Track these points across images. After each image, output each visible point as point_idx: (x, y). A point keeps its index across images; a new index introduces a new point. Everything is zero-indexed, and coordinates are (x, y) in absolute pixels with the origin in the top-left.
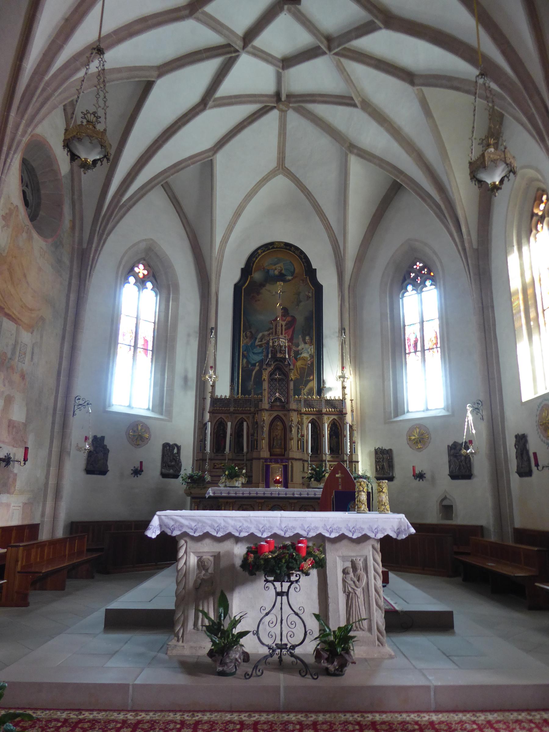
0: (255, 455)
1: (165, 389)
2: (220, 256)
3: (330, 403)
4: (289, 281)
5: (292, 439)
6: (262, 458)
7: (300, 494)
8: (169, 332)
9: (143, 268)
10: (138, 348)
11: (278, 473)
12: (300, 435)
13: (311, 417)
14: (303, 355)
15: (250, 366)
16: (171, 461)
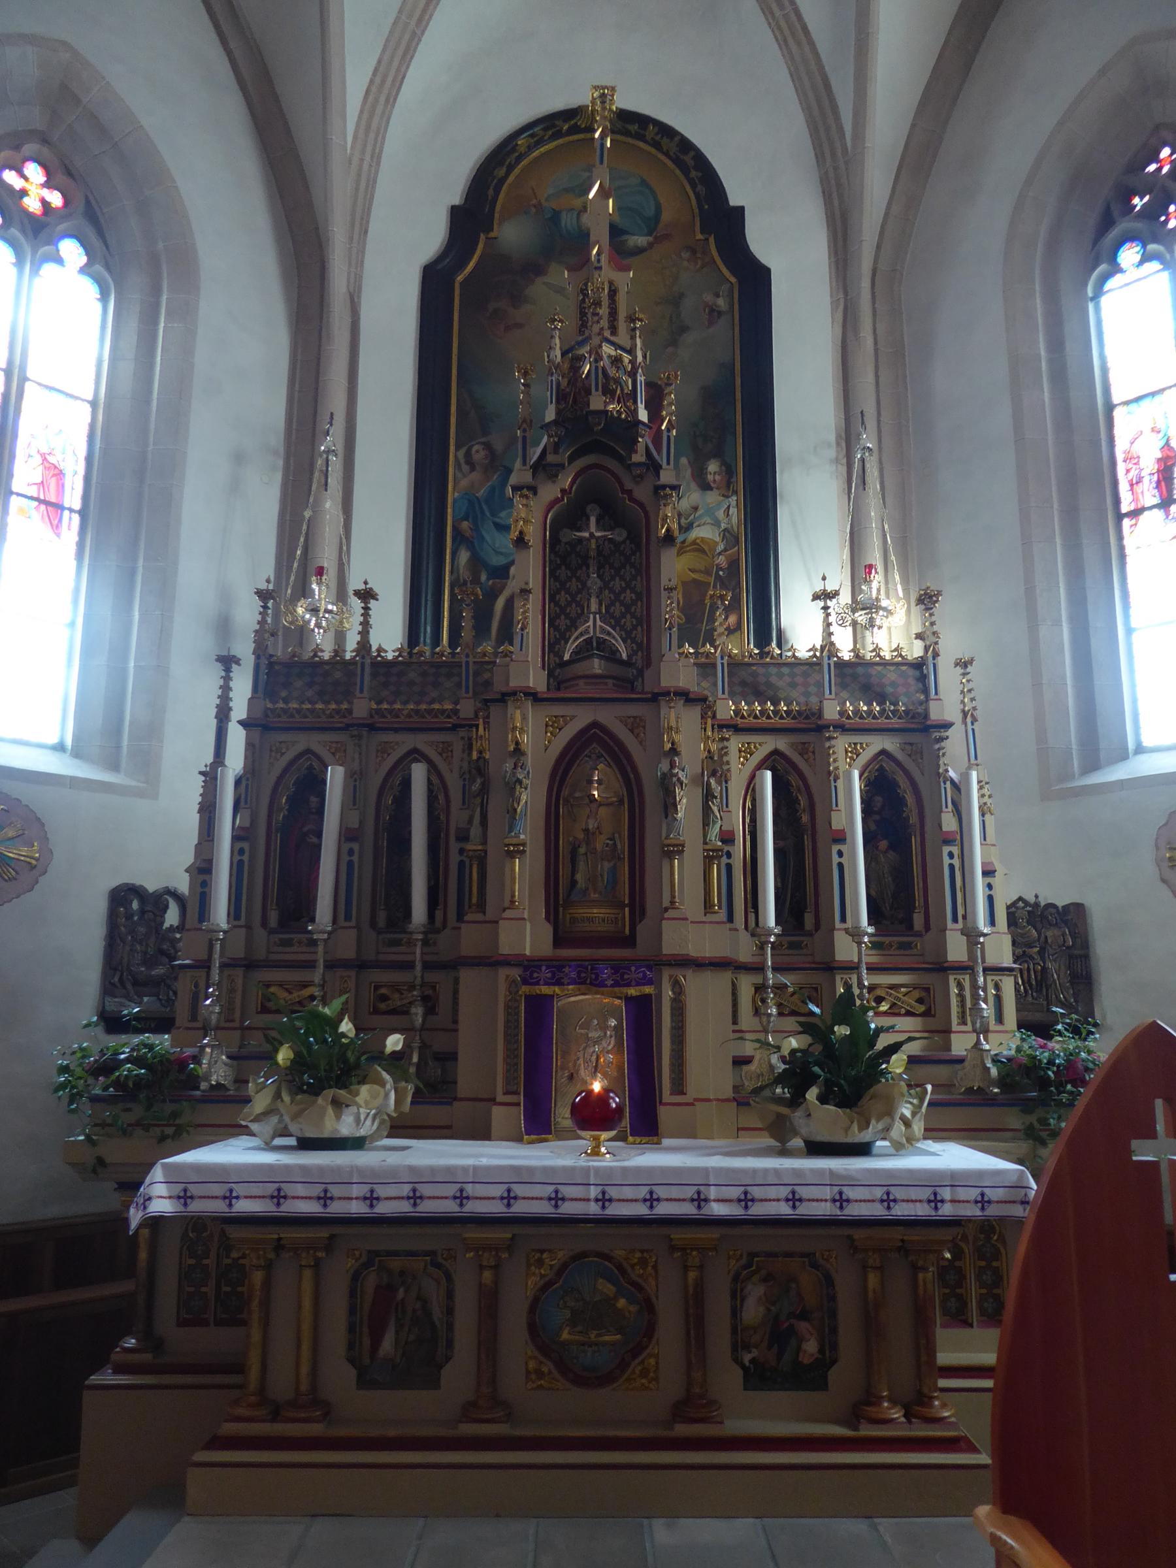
0: (470, 940)
1: (132, 664)
2: (363, 152)
3: (855, 677)
4: (639, 251)
5: (673, 851)
6: (506, 962)
7: (746, 1200)
8: (151, 439)
9: (43, 179)
10: (12, 493)
11: (597, 1042)
12: (714, 832)
13: (767, 745)
14: (696, 533)
15: (483, 577)
16: (150, 962)
